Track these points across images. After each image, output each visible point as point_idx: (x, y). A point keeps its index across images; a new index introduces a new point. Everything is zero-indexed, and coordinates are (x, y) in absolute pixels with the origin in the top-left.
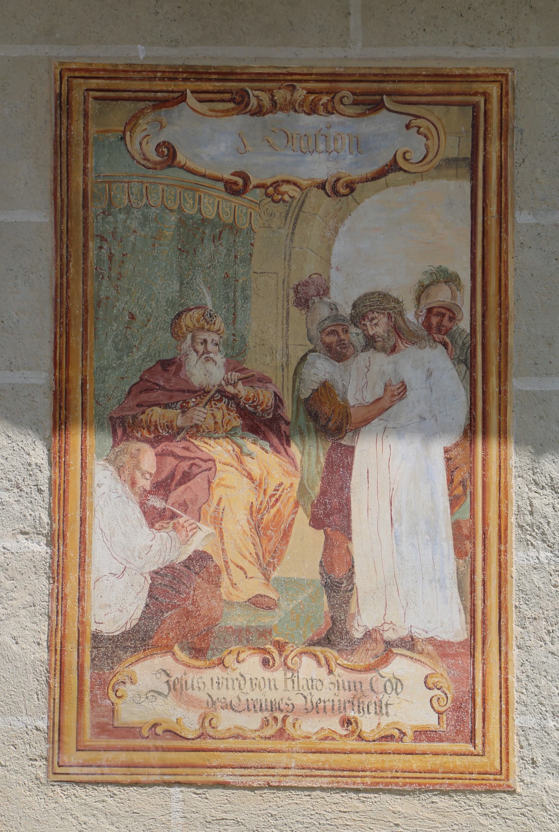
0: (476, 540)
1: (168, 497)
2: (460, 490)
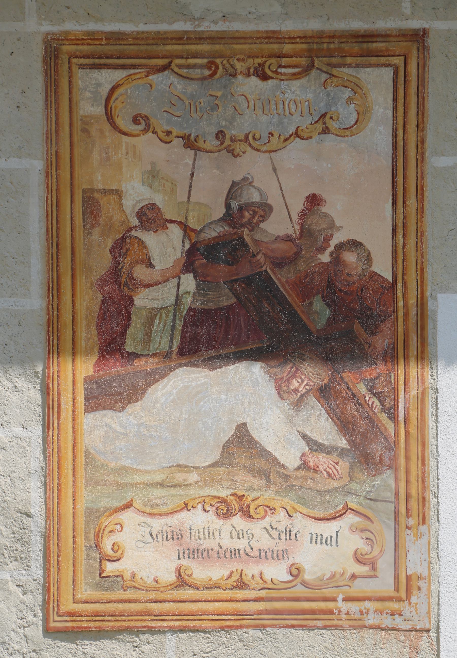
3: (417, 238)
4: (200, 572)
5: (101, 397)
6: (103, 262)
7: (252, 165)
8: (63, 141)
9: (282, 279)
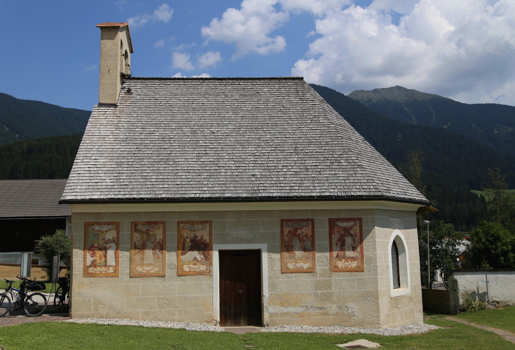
0: (117, 258)
1: (93, 255)
2: (115, 254)
4: (191, 270)
5: (182, 254)
6: (182, 242)
7: (196, 232)
8: (179, 230)
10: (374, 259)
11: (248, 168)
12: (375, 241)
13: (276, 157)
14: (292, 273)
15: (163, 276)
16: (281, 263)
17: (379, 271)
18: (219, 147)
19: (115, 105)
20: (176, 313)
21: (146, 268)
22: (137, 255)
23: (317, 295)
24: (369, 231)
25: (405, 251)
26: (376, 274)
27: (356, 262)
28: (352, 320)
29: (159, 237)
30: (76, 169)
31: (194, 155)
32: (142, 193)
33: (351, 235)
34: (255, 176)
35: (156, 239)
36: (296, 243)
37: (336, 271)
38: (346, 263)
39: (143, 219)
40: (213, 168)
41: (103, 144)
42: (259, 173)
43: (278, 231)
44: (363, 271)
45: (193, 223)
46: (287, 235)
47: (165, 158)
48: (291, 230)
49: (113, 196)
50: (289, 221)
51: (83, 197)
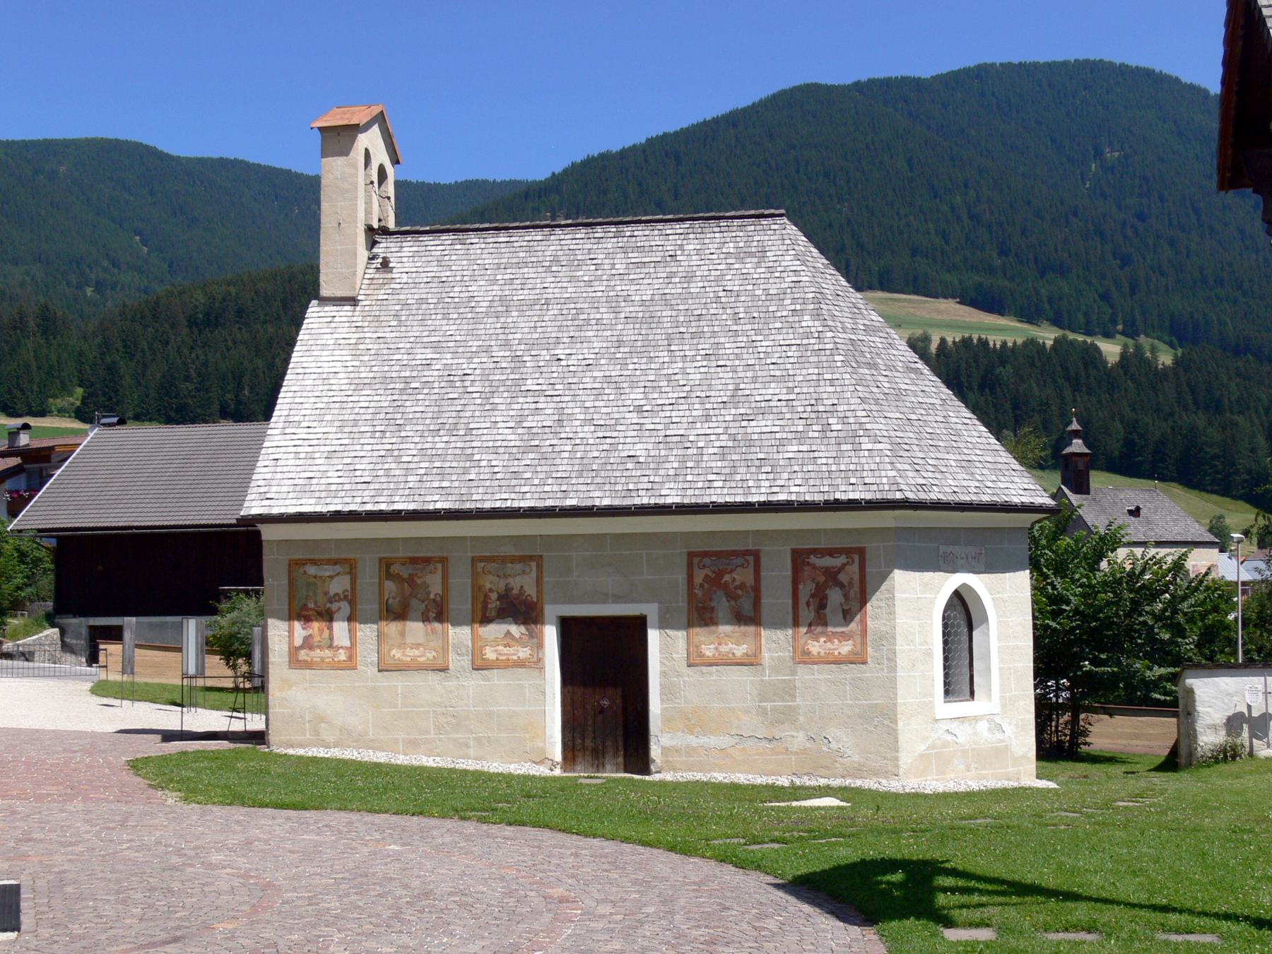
3: (1191, 912)
6: (482, 599)
7: (510, 580)
8: (475, 575)
9: (516, 602)
10: (888, 638)
11: (622, 441)
12: (893, 598)
13: (688, 413)
14: (711, 665)
15: (444, 670)
16: (688, 644)
17: (901, 661)
18: (567, 392)
19: (353, 301)
20: (471, 743)
21: (409, 652)
22: (392, 628)
23: (763, 712)
24: (884, 576)
25: (985, 619)
26: (893, 669)
27: (850, 642)
28: (837, 765)
29: (436, 588)
30: (270, 450)
31: (511, 413)
32: (397, 499)
33: (841, 586)
34: (635, 460)
35: (429, 593)
36: (722, 605)
37: (805, 663)
38: (829, 645)
39: (401, 553)
40: (548, 443)
41: (324, 393)
42: (643, 453)
43: (681, 577)
44: (864, 663)
45: (503, 560)
46: (701, 586)
47: (450, 421)
48: (710, 574)
49: (339, 508)
50: (706, 554)
51: (283, 510)
